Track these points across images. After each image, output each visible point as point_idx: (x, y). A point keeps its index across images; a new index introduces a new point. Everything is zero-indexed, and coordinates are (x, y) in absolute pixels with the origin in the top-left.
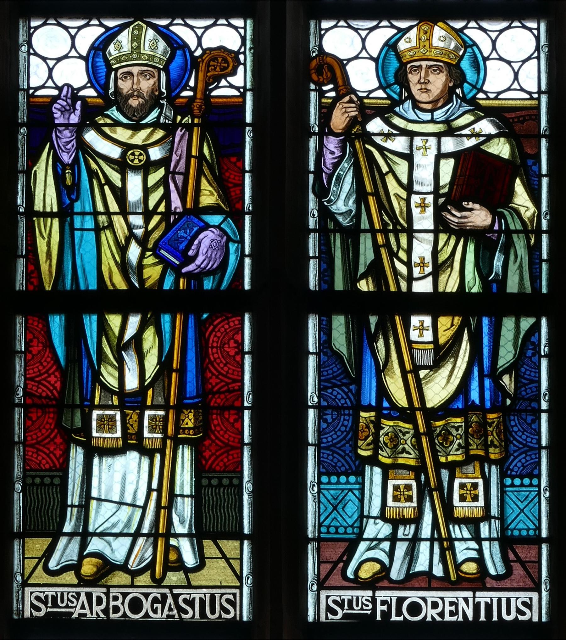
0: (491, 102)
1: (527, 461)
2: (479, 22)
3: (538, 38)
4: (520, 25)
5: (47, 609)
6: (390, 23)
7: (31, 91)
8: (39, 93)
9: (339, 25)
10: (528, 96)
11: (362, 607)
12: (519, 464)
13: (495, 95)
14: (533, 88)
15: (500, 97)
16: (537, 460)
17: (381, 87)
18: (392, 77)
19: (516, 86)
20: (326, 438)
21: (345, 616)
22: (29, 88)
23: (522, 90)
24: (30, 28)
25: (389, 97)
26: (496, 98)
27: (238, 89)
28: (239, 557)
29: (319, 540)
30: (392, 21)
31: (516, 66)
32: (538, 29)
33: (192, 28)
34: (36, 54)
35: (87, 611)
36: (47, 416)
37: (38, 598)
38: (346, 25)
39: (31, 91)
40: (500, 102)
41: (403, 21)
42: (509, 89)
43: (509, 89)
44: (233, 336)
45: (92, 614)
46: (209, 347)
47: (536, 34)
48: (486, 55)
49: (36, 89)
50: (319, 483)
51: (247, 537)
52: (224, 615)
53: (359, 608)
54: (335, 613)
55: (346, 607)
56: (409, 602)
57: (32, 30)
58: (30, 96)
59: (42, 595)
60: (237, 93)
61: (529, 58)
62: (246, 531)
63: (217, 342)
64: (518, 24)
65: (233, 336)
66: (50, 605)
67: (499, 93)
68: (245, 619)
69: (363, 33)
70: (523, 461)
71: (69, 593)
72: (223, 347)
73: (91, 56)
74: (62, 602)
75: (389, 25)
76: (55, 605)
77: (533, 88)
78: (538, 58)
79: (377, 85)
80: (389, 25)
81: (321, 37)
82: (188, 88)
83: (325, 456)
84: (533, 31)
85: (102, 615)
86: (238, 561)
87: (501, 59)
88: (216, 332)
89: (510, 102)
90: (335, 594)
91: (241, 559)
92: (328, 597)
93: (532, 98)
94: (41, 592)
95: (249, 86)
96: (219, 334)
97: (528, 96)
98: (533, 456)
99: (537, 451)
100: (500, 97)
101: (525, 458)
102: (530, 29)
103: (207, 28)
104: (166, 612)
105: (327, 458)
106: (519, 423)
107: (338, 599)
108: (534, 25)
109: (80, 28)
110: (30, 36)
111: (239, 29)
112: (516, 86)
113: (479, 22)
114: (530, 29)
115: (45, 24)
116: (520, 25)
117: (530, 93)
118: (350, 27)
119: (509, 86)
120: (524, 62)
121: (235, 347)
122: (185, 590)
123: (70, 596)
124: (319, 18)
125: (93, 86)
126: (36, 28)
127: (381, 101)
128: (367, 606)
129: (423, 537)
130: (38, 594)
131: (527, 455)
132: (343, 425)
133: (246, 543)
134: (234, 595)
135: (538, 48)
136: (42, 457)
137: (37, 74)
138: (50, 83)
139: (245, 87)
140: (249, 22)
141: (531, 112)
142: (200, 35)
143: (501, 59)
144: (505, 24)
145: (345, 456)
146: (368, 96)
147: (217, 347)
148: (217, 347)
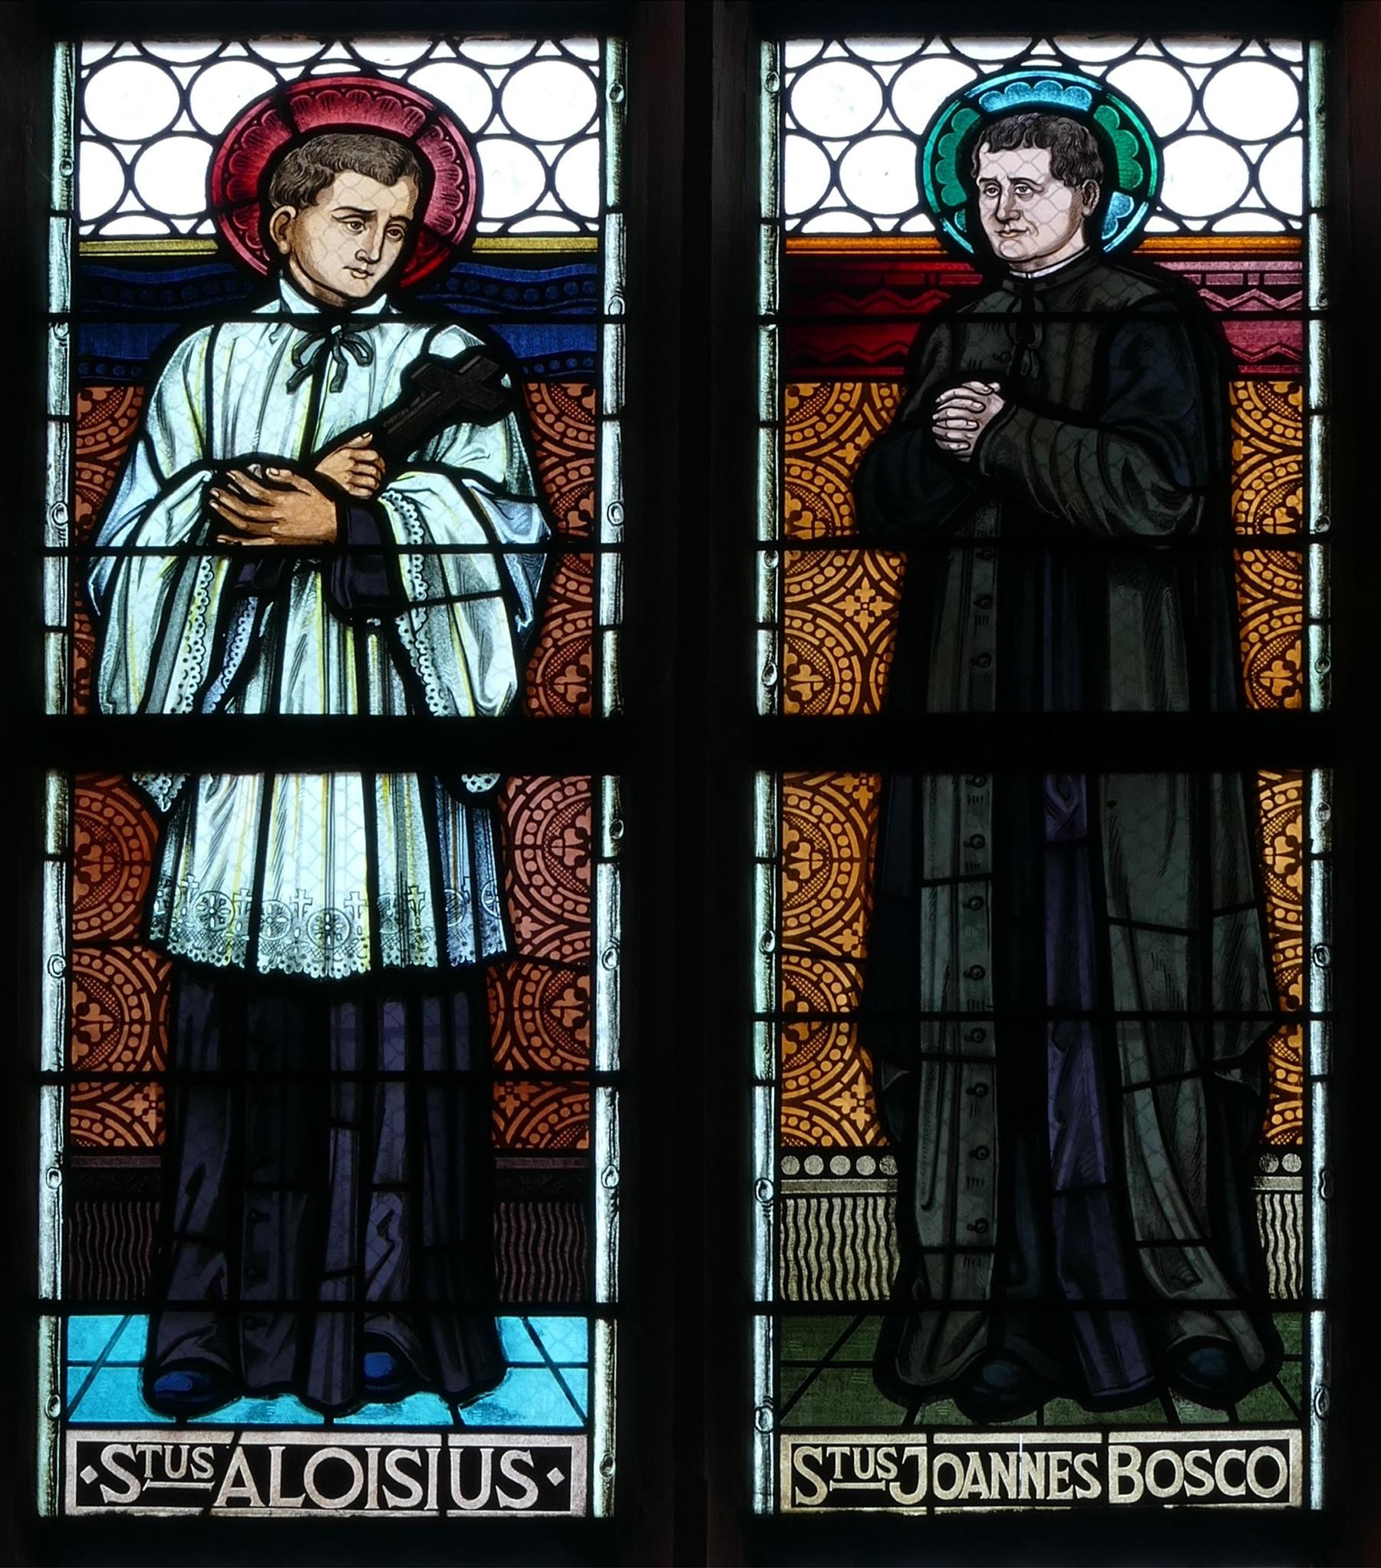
0: (883, 242)
1: (562, 1119)
2: (564, 43)
3: (1303, 87)
4: (945, 50)
6: (1265, 47)
7: (790, 225)
9: (1139, 52)
10: (575, 228)
11: (1215, 1457)
12: (543, 1128)
13: (1204, 223)
14: (589, 208)
15: (512, 230)
17: (923, 207)
18: (254, 181)
19: (549, 203)
20: (578, 793)
21: (833, 1498)
23: (851, 208)
24: (80, 67)
25: (939, 234)
28: (585, 1359)
29: (779, 1309)
31: (550, 153)
32: (1304, 64)
34: (801, 131)
37: (809, 1461)
38: (1159, 53)
39: (790, 225)
40: (907, 242)
41: (1083, 41)
42: (1236, 209)
43: (1236, 209)
44: (574, 818)
47: (1300, 77)
48: (473, 128)
50: (779, 1174)
51: (606, 1312)
52: (1190, 1490)
53: (183, 1471)
54: (809, 1489)
55: (838, 1475)
56: (400, 1473)
57: (85, 74)
58: (785, 235)
62: (601, 1294)
63: (535, 835)
65: (574, 818)
67: (1213, 219)
68: (599, 1511)
69: (887, 73)
70: (553, 1119)
71: (878, 1447)
72: (550, 847)
73: (933, 138)
74: (864, 1469)
75: (559, 53)
76: (849, 1475)
77: (589, 208)
78: (1305, 134)
79: (913, 201)
80: (559, 53)
81: (82, 84)
82: (1159, 209)
84: (1293, 69)
86: (585, 1370)
87: (514, 136)
88: (532, 811)
89: (833, 242)
90: (812, 1444)
91: (590, 1365)
92: (795, 1447)
93: (585, 232)
94: (816, 1446)
96: (538, 815)
97: (575, 228)
98: (577, 1108)
99: (586, 1096)
100: (512, 230)
101: (556, 1112)
102: (584, 65)
103: (1216, 67)
105: (90, 1130)
106: (546, 1028)
107: (128, 1451)
111: (1105, 68)
113: (564, 43)
114: (584, 65)
116: (947, 51)
117: (1284, 218)
118: (1168, 58)
119: (532, 203)
120: (1272, 142)
121: (577, 847)
123: (392, 1471)
124: (780, 38)
126: (96, 67)
127: (1267, 241)
128: (887, 1470)
130: (811, 1451)
131: (561, 1106)
132: (126, 1047)
133: (601, 1327)
135: (1303, 113)
136: (116, 1132)
137: (803, 179)
138: (549, 203)
140: (1314, 52)
141: (574, 270)
143: (514, 136)
145: (132, 1122)
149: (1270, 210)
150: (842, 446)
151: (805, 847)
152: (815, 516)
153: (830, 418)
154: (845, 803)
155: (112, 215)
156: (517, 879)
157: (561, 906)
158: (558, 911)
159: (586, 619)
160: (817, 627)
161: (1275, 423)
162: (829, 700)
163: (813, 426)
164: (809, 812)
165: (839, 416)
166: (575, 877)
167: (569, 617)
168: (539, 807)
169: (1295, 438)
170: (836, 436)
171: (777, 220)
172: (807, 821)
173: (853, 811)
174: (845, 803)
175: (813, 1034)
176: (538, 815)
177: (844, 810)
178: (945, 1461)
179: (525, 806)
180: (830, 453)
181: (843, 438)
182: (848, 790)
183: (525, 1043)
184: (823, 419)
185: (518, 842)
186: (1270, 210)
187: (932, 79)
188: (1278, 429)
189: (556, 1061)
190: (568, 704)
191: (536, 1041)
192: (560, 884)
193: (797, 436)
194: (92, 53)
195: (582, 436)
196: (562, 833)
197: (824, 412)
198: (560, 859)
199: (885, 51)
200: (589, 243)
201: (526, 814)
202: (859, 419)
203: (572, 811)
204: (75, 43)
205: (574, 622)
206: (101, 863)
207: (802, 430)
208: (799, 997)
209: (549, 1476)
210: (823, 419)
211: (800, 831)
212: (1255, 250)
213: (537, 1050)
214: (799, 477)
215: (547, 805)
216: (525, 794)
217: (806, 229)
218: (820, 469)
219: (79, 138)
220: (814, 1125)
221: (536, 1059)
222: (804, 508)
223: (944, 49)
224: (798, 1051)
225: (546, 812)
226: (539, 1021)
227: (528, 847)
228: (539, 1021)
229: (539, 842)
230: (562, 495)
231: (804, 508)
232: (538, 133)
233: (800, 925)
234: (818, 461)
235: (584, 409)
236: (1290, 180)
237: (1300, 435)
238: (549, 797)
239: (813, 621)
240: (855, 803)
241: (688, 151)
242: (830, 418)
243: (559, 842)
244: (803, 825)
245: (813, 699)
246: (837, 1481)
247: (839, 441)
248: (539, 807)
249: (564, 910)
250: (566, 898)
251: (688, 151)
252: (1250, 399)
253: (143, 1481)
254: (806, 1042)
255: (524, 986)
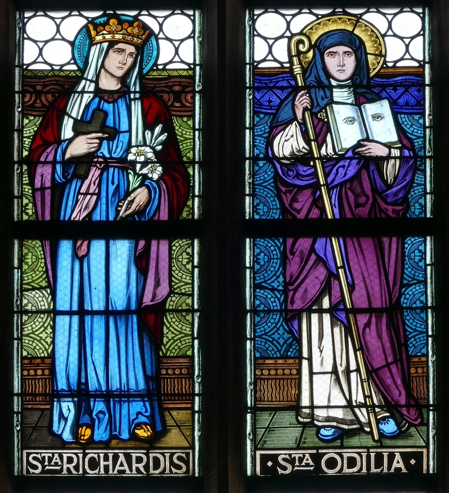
3: (194, 22)
5: (293, 468)
7: (25, 67)
8: (261, 66)
10: (279, 66)
13: (393, 63)
16: (425, 341)
19: (407, 56)
20: (260, 329)
22: (254, 61)
23: (412, 59)
26: (61, 70)
27: (418, 61)
30: (81, 12)
32: (194, 15)
33: (155, 17)
34: (29, 39)
35: (126, 467)
36: (39, 316)
39: (25, 67)
42: (402, 59)
44: (261, 320)
45: (113, 471)
46: (405, 256)
49: (29, 65)
58: (24, 70)
59: (39, 456)
60: (417, 64)
61: (282, 37)
64: (77, 13)
65: (261, 320)
66: (46, 463)
67: (62, 66)
72: (268, 259)
83: (259, 343)
85: (74, 472)
88: (274, 322)
94: (37, 453)
95: (197, 62)
97: (279, 66)
98: (422, 339)
103: (63, 18)
104: (117, 468)
108: (191, 13)
109: (63, 18)
110: (254, 21)
112: (40, 59)
114: (418, 14)
115: (34, 16)
116: (147, 14)
117: (281, 63)
120: (412, 38)
122: (407, 449)
125: (76, 63)
126: (259, 15)
129: (303, 405)
134: (188, 454)
135: (423, 29)
139: (424, 60)
142: (161, 23)
144: (66, 13)
146: (61, 68)
147: (274, 259)
148: (274, 259)
149: (182, 62)
150: (173, 338)
151: (184, 263)
152: (182, 263)
153: (176, 347)
154: (171, 328)
155: (264, 60)
156: (279, 248)
157: (265, 191)
158: (265, 189)
159: (257, 181)
160: (181, 132)
161: (414, 129)
162: (177, 252)
163: (182, 345)
164: (183, 274)
165: (174, 348)
166: (260, 249)
167: (262, 181)
168: (272, 324)
169: (421, 133)
170: (175, 341)
171: (21, 66)
172: (183, 271)
173: (168, 326)
174: (171, 328)
175: (181, 305)
176: (272, 321)
177: (171, 326)
178: (282, 461)
179: (276, 272)
180: (177, 335)
181: (172, 341)
182: (170, 333)
183: (276, 247)
184: (179, 347)
185: (279, 260)
186: (182, 62)
187: (73, 24)
188: (415, 131)
189: (266, 243)
190: (416, 215)
191: (272, 300)
192: (265, 198)
193: (187, 341)
194: (257, 12)
195: (419, 132)
196: (265, 263)
197: (178, 350)
198: (265, 255)
199: (58, 15)
200: (191, 72)
201: (276, 270)
202: (167, 347)
203: (262, 322)
204: (22, 12)
205: (261, 180)
206: (415, 256)
207: (186, 343)
208: (186, 122)
209: (272, 464)
210: (179, 347)
211: (185, 268)
212: (407, 72)
213: (272, 245)
214: (187, 276)
215: (269, 324)
216: (276, 276)
217: (63, 69)
218: (180, 278)
219: (254, 35)
220: (181, 132)
221: (273, 243)
222: (185, 265)
223: (77, 13)
224: (186, 249)
225: (270, 322)
226: (272, 254)
227: (275, 259)
228: (272, 254)
229: (272, 210)
230: (413, 198)
231: (185, 265)
232: (177, 38)
233: (186, 143)
234: (181, 333)
235: (419, 123)
236: (418, 49)
237: (422, 132)
238: (269, 275)
239: (183, 134)
240: (168, 328)
241: (224, 44)
242: (176, 347)
243: (265, 210)
244: (186, 271)
245: (182, 304)
246: (298, 466)
247: (174, 340)
248: (272, 324)
249: (263, 190)
250: (263, 193)
251: (224, 44)
252: (406, 121)
253: (293, 467)
254: (183, 303)
255: (277, 256)
